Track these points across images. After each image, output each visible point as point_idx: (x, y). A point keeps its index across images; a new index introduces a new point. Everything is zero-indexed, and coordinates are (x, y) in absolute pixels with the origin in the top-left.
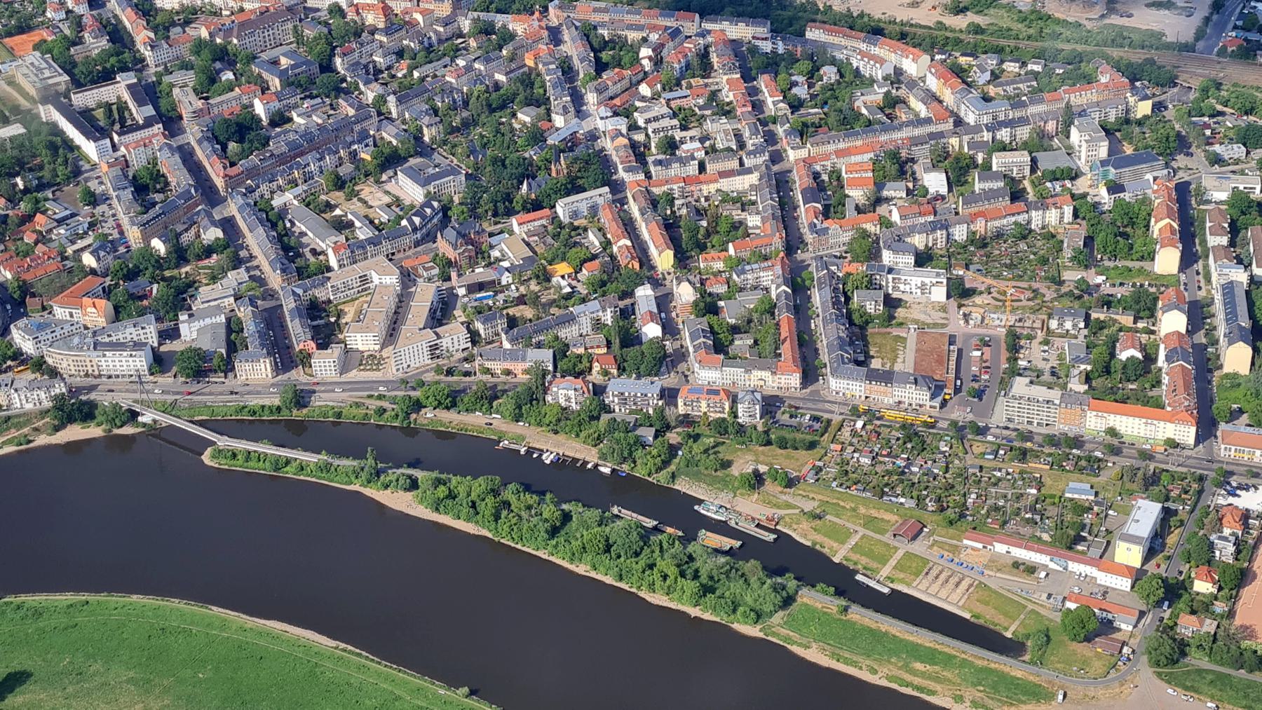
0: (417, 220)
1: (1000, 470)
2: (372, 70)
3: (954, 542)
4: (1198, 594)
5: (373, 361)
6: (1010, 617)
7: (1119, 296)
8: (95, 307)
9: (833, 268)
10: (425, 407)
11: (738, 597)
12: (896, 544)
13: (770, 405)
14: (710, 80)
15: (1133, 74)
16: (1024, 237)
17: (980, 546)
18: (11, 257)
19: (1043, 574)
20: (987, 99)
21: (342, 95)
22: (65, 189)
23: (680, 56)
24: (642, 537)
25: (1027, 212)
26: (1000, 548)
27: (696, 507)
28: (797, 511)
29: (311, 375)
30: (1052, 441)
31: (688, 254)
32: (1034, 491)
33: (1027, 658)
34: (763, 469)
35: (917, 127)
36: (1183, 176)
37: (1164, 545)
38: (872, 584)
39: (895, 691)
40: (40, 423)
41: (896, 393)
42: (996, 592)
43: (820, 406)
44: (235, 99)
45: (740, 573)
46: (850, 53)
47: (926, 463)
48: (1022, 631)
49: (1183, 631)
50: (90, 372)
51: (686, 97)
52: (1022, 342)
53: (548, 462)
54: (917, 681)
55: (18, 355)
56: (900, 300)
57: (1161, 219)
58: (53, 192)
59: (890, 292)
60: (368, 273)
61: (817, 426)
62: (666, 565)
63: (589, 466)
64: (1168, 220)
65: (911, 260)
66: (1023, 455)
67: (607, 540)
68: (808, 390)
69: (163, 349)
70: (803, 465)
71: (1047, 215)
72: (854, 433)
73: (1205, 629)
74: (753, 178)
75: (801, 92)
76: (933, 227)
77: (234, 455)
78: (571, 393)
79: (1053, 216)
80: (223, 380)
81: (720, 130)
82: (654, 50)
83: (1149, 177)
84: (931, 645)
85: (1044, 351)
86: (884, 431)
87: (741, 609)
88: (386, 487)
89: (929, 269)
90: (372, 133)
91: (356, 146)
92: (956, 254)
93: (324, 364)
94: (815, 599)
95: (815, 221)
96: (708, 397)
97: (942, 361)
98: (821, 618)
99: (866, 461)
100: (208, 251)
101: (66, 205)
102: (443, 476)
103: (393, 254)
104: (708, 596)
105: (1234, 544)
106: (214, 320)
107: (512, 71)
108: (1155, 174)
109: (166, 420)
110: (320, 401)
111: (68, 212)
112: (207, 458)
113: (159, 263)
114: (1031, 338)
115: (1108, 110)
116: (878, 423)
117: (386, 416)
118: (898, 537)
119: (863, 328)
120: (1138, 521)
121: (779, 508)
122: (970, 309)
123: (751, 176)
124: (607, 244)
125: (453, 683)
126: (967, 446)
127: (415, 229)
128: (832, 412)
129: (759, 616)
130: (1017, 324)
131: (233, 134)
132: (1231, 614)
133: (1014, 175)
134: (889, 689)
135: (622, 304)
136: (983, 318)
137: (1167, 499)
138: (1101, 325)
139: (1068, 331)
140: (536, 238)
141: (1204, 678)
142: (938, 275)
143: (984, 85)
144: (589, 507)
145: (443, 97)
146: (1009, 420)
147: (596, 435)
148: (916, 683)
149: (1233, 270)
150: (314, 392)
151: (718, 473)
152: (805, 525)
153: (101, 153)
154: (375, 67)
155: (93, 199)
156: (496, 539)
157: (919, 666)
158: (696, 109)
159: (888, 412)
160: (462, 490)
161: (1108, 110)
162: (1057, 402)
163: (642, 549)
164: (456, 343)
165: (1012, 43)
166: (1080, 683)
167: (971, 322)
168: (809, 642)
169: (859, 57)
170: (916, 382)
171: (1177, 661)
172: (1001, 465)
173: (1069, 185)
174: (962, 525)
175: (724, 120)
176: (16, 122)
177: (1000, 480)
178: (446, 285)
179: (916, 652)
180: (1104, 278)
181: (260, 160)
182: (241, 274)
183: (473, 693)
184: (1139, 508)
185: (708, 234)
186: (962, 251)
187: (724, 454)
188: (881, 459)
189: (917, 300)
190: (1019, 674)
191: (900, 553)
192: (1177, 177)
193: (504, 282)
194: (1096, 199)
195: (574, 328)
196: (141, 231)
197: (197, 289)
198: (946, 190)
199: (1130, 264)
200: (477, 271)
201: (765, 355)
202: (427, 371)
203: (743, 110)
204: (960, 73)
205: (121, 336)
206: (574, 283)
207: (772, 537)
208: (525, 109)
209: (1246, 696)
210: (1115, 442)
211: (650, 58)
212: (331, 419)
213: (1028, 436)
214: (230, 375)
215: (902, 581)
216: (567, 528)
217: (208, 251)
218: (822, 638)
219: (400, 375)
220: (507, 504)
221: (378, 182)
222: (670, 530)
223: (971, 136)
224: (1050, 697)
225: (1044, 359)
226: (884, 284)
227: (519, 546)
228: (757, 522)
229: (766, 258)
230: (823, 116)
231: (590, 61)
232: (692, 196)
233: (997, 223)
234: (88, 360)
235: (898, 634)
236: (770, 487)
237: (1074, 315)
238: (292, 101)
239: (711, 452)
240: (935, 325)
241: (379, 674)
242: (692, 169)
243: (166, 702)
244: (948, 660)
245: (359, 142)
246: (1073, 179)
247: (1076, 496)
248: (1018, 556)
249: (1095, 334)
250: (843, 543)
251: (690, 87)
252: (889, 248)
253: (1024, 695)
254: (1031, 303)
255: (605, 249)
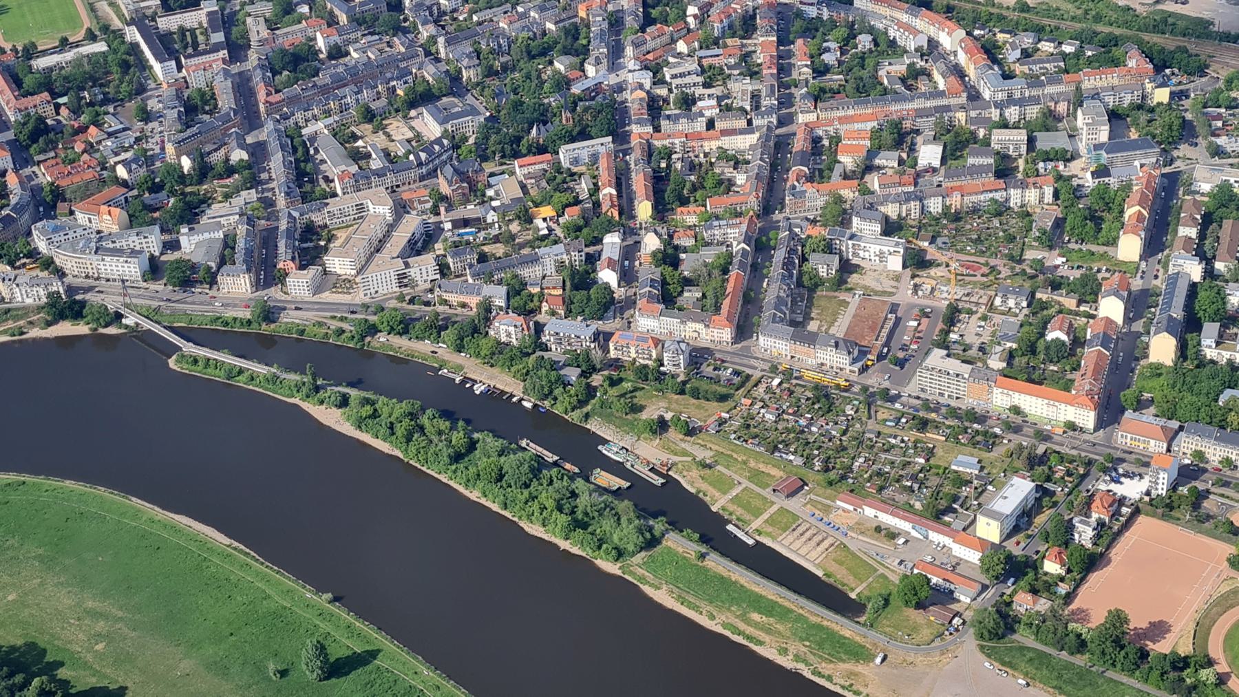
0: (423, 156)
1: (895, 437)
2: (436, 11)
3: (828, 502)
4: (1046, 574)
5: (346, 284)
6: (860, 579)
7: (1072, 278)
8: (110, 214)
9: (797, 230)
10: (380, 331)
11: (608, 534)
12: (774, 499)
13: (698, 356)
14: (749, 41)
15: (1160, 63)
16: (999, 214)
17: (851, 508)
18: (57, 164)
19: (901, 541)
20: (1008, 76)
21: (400, 34)
22: (127, 104)
23: (723, 16)
24: (532, 469)
25: (1006, 190)
26: (869, 512)
27: (600, 447)
28: (689, 459)
29: (286, 293)
30: (954, 412)
31: (669, 206)
32: (922, 461)
33: (862, 619)
34: (668, 416)
35: (928, 99)
36: (1179, 165)
37: (1030, 523)
38: (740, 534)
39: (727, 638)
40: (35, 318)
41: (818, 355)
42: (853, 554)
43: (745, 361)
44: (301, 31)
45: (613, 512)
46: (889, 23)
47: (827, 424)
48: (866, 593)
49: (1018, 608)
50: (91, 274)
51: (718, 56)
52: (962, 316)
53: (477, 392)
54: (750, 630)
55: (33, 254)
56: (858, 266)
57: (1133, 206)
58: (115, 108)
59: (851, 257)
60: (364, 202)
61: (737, 380)
62: (547, 497)
63: (514, 399)
64: (1138, 208)
65: (877, 228)
66: (923, 425)
67: (501, 468)
68: (739, 346)
69: (163, 258)
70: (709, 416)
71: (1027, 194)
72: (769, 390)
73: (1038, 608)
74: (753, 139)
75: (829, 58)
76: (908, 198)
77: (196, 361)
78: (512, 329)
79: (1033, 195)
80: (207, 291)
81: (741, 88)
82: (700, 9)
83: (1137, 163)
84: (773, 598)
85: (980, 327)
86: (799, 390)
87: (605, 546)
88: (322, 402)
89: (896, 239)
90: (414, 71)
91: (395, 83)
92: (931, 226)
93: (299, 284)
94: (679, 544)
95: (796, 183)
96: (637, 343)
97: (876, 329)
98: (679, 562)
99: (771, 417)
100: (230, 171)
101: (122, 120)
102: (373, 397)
103: (398, 186)
104: (578, 530)
105: (1094, 529)
106: (212, 235)
107: (561, 21)
108: (1143, 161)
109: (147, 325)
110: (289, 318)
111: (121, 126)
112: (172, 363)
113: (182, 179)
114: (970, 313)
115: (1122, 95)
116: (794, 382)
117: (343, 336)
118: (777, 493)
119: (812, 290)
120: (1006, 498)
121: (676, 454)
122: (923, 280)
123: (752, 136)
124: (596, 189)
125: (320, 589)
126: (872, 412)
127: (420, 164)
128: (755, 368)
129: (620, 554)
130: (964, 298)
131: (288, 63)
132: (1069, 598)
133: (1011, 153)
134: (721, 635)
135: (591, 250)
136: (933, 290)
137: (1048, 479)
138: (1044, 306)
139: (1010, 309)
140: (533, 181)
141: (1025, 655)
142: (897, 244)
143: (1014, 62)
144: (499, 437)
145: (488, 41)
146: (923, 390)
147: (525, 371)
148: (747, 632)
149: (1187, 262)
150: (285, 309)
151: (629, 417)
152: (695, 473)
153: (165, 73)
154: (439, 9)
155: (146, 116)
156: (406, 460)
157: (756, 617)
158: (725, 68)
159: (811, 374)
160: (385, 411)
161: (1122, 95)
162: (966, 376)
163: (531, 481)
164: (424, 274)
165: (1053, 23)
166: (903, 648)
167: (920, 293)
168: (661, 584)
169: (896, 28)
170: (837, 345)
171: (1003, 636)
172: (899, 432)
173: (1061, 167)
174: (843, 487)
175: (748, 80)
176: (102, 40)
177: (893, 447)
178: (433, 219)
179: (758, 603)
180: (1064, 260)
181: (302, 89)
182: (251, 195)
183: (336, 599)
184: (1012, 485)
185: (694, 189)
186: (933, 223)
187: (640, 399)
188: (786, 417)
189: (874, 268)
190: (847, 634)
191: (775, 508)
192: (1173, 166)
193: (489, 220)
194: (1081, 182)
195: (537, 268)
196: (176, 148)
197: (209, 206)
198: (939, 163)
199: (1094, 248)
200: (469, 207)
201: (709, 308)
202: (392, 298)
203: (769, 72)
204: (991, 52)
205: (124, 244)
206: (554, 226)
207: (659, 481)
208: (562, 58)
209: (1060, 676)
210: (1019, 420)
211: (695, 16)
212: (294, 336)
213: (927, 405)
214: (215, 287)
215: (769, 535)
216: (471, 456)
217: (230, 171)
218: (674, 581)
219: (367, 300)
220: (422, 429)
221: (405, 117)
222: (568, 466)
223: (978, 112)
224: (870, 658)
225: (978, 335)
226: (844, 249)
227: (424, 469)
228: (651, 466)
229: (739, 215)
230: (844, 83)
231: (637, 16)
232: (694, 151)
233: (974, 198)
234: (88, 262)
235: (746, 584)
236: (673, 434)
237: (1018, 294)
238: (353, 36)
239: (628, 396)
240: (884, 293)
241: (257, 574)
242: (700, 125)
243: (62, 579)
244: (783, 614)
245: (398, 79)
246: (1067, 161)
247: (961, 469)
248: (884, 521)
249: (1033, 314)
250: (725, 493)
251: (725, 46)
252: (858, 214)
253: (845, 654)
254: (985, 279)
255: (591, 195)
